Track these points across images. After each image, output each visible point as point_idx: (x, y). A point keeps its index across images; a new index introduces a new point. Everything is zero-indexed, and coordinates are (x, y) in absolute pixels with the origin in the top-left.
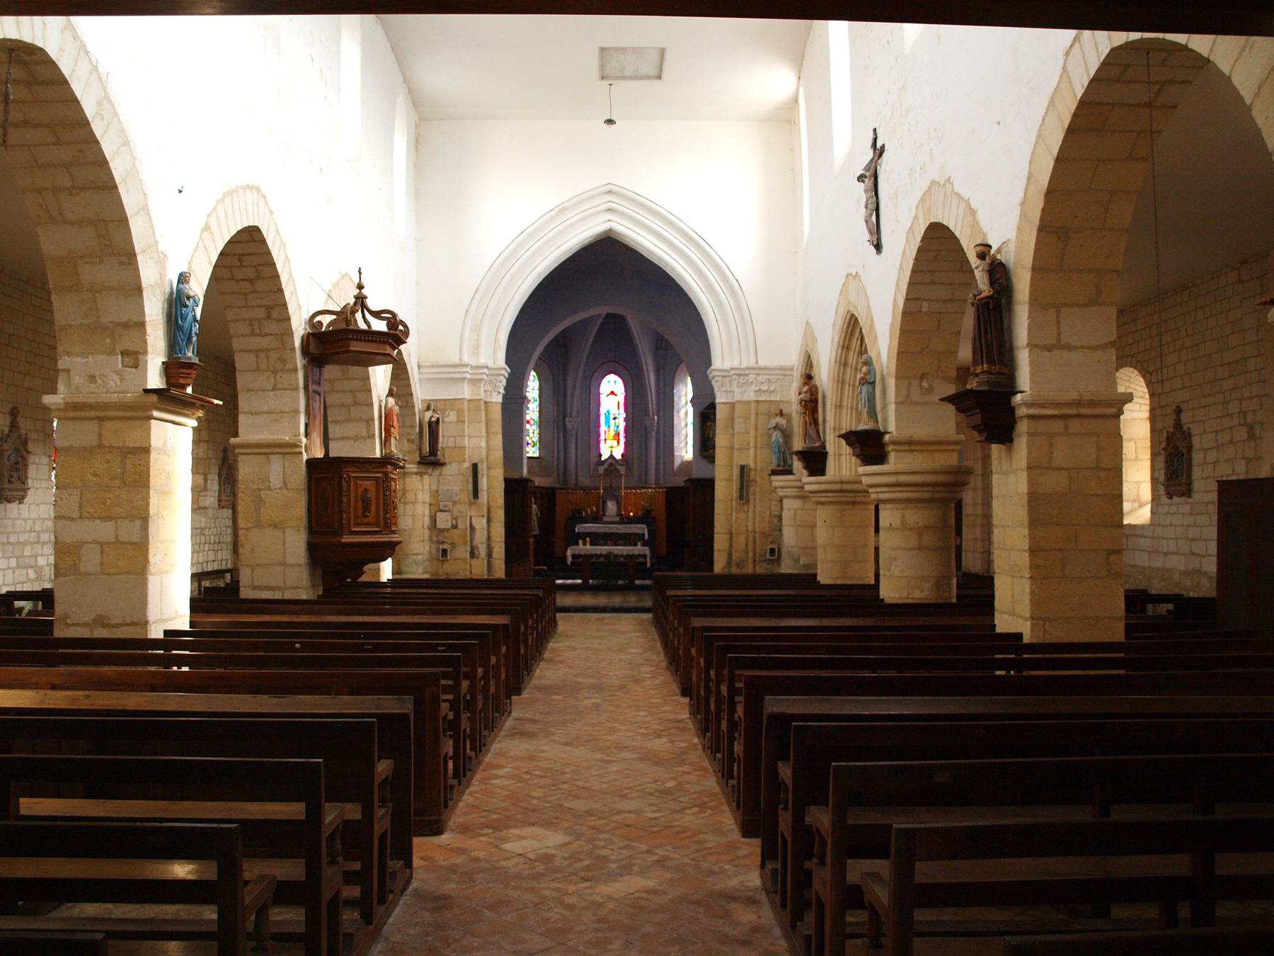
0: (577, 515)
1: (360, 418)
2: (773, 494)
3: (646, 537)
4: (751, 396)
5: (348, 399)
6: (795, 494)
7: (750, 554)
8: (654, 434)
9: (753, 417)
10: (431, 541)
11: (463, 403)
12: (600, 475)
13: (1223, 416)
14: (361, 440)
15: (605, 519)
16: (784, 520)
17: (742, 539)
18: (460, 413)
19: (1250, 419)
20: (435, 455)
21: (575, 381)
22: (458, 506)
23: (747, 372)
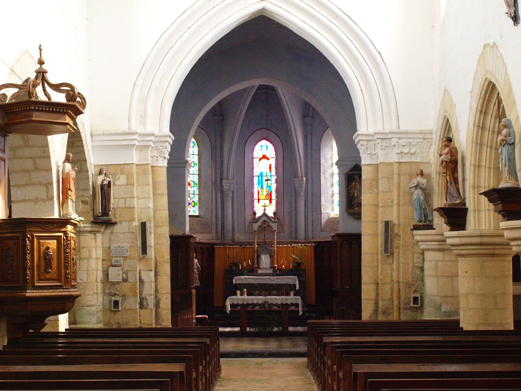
0: (234, 268)
1: (40, 182)
2: (415, 247)
3: (297, 287)
5: (29, 164)
6: (436, 247)
7: (396, 303)
8: (303, 194)
9: (396, 177)
10: (104, 293)
11: (132, 168)
12: (255, 231)
14: (41, 203)
15: (260, 271)
16: (425, 271)
17: (387, 288)
18: (129, 176)
20: (107, 215)
21: (231, 148)
22: (128, 261)
23: (390, 136)
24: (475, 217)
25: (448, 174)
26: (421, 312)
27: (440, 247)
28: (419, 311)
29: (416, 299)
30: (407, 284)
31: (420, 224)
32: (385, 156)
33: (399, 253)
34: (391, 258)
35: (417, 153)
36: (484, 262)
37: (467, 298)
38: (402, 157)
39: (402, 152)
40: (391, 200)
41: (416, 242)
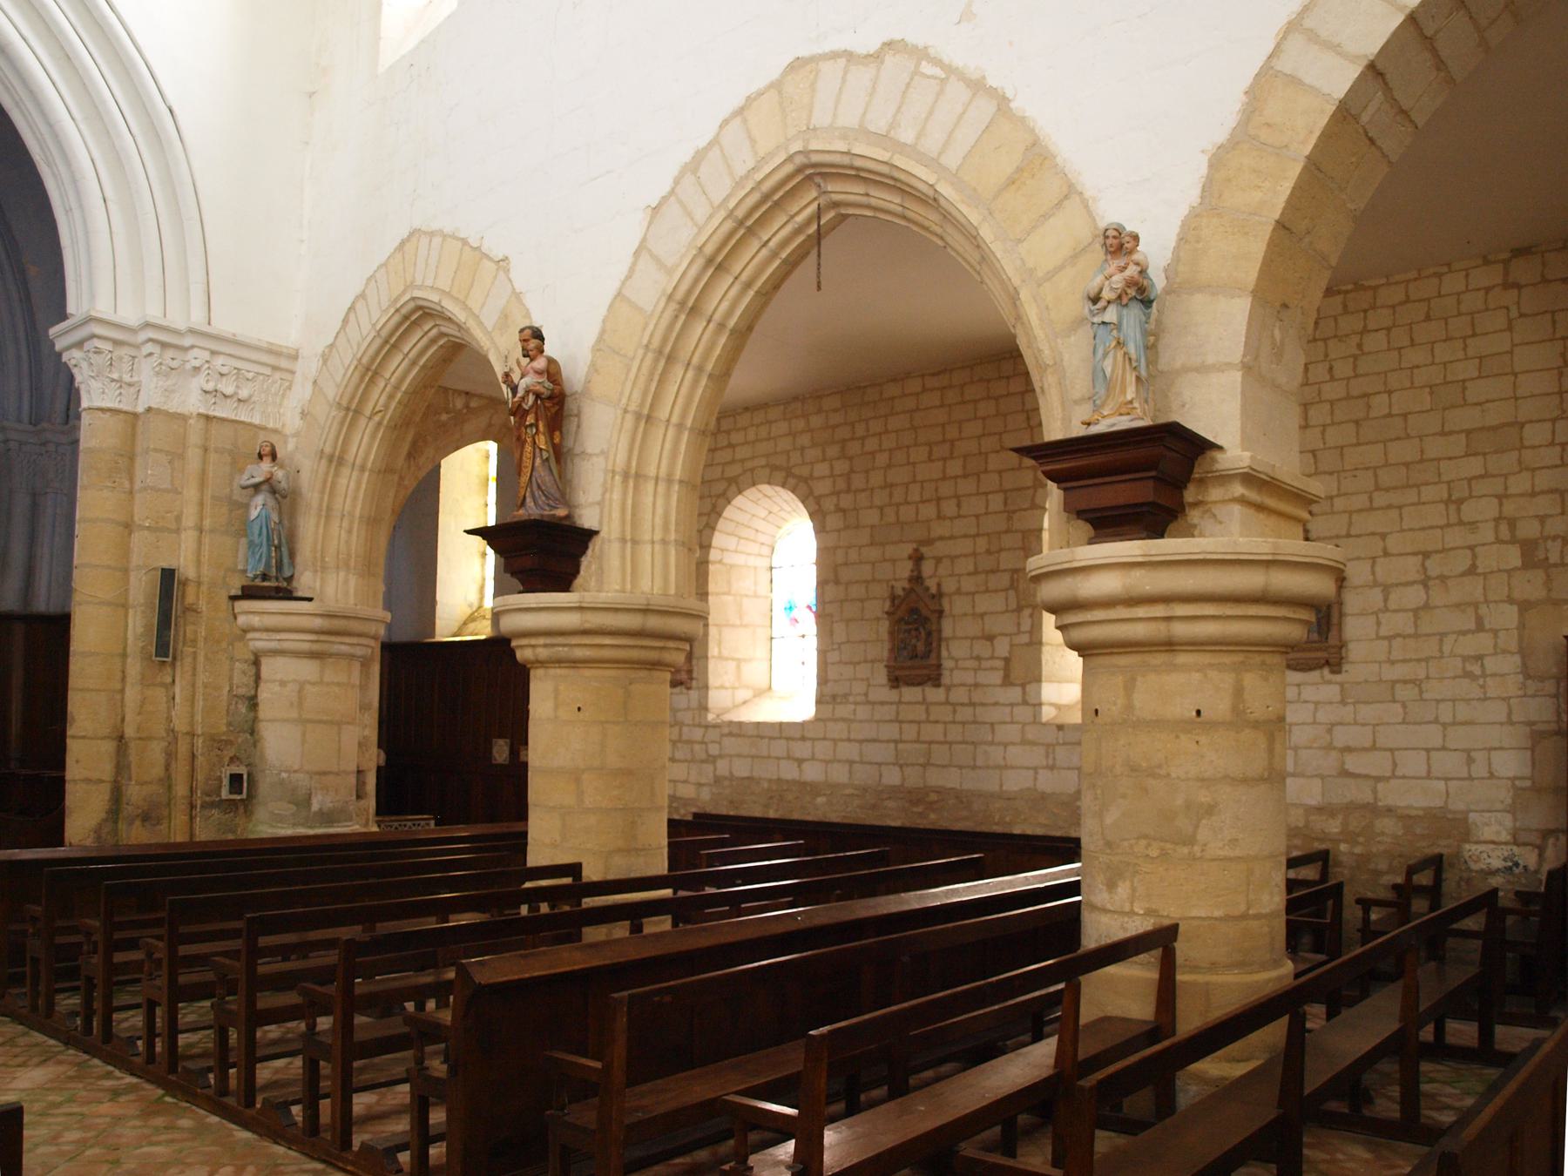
2: (238, 645)
4: (190, 400)
6: (306, 646)
7: (181, 790)
9: (193, 454)
13: (1448, 525)
16: (261, 707)
17: (156, 751)
19: (1529, 530)
23: (187, 342)
24: (623, 558)
25: (541, 428)
26: (245, 812)
27: (315, 647)
28: (241, 810)
29: (236, 780)
30: (214, 740)
31: (266, 584)
32: (167, 394)
33: (195, 658)
34: (169, 670)
35: (254, 402)
36: (630, 684)
37: (578, 780)
38: (215, 403)
39: (216, 391)
40: (175, 513)
41: (239, 632)
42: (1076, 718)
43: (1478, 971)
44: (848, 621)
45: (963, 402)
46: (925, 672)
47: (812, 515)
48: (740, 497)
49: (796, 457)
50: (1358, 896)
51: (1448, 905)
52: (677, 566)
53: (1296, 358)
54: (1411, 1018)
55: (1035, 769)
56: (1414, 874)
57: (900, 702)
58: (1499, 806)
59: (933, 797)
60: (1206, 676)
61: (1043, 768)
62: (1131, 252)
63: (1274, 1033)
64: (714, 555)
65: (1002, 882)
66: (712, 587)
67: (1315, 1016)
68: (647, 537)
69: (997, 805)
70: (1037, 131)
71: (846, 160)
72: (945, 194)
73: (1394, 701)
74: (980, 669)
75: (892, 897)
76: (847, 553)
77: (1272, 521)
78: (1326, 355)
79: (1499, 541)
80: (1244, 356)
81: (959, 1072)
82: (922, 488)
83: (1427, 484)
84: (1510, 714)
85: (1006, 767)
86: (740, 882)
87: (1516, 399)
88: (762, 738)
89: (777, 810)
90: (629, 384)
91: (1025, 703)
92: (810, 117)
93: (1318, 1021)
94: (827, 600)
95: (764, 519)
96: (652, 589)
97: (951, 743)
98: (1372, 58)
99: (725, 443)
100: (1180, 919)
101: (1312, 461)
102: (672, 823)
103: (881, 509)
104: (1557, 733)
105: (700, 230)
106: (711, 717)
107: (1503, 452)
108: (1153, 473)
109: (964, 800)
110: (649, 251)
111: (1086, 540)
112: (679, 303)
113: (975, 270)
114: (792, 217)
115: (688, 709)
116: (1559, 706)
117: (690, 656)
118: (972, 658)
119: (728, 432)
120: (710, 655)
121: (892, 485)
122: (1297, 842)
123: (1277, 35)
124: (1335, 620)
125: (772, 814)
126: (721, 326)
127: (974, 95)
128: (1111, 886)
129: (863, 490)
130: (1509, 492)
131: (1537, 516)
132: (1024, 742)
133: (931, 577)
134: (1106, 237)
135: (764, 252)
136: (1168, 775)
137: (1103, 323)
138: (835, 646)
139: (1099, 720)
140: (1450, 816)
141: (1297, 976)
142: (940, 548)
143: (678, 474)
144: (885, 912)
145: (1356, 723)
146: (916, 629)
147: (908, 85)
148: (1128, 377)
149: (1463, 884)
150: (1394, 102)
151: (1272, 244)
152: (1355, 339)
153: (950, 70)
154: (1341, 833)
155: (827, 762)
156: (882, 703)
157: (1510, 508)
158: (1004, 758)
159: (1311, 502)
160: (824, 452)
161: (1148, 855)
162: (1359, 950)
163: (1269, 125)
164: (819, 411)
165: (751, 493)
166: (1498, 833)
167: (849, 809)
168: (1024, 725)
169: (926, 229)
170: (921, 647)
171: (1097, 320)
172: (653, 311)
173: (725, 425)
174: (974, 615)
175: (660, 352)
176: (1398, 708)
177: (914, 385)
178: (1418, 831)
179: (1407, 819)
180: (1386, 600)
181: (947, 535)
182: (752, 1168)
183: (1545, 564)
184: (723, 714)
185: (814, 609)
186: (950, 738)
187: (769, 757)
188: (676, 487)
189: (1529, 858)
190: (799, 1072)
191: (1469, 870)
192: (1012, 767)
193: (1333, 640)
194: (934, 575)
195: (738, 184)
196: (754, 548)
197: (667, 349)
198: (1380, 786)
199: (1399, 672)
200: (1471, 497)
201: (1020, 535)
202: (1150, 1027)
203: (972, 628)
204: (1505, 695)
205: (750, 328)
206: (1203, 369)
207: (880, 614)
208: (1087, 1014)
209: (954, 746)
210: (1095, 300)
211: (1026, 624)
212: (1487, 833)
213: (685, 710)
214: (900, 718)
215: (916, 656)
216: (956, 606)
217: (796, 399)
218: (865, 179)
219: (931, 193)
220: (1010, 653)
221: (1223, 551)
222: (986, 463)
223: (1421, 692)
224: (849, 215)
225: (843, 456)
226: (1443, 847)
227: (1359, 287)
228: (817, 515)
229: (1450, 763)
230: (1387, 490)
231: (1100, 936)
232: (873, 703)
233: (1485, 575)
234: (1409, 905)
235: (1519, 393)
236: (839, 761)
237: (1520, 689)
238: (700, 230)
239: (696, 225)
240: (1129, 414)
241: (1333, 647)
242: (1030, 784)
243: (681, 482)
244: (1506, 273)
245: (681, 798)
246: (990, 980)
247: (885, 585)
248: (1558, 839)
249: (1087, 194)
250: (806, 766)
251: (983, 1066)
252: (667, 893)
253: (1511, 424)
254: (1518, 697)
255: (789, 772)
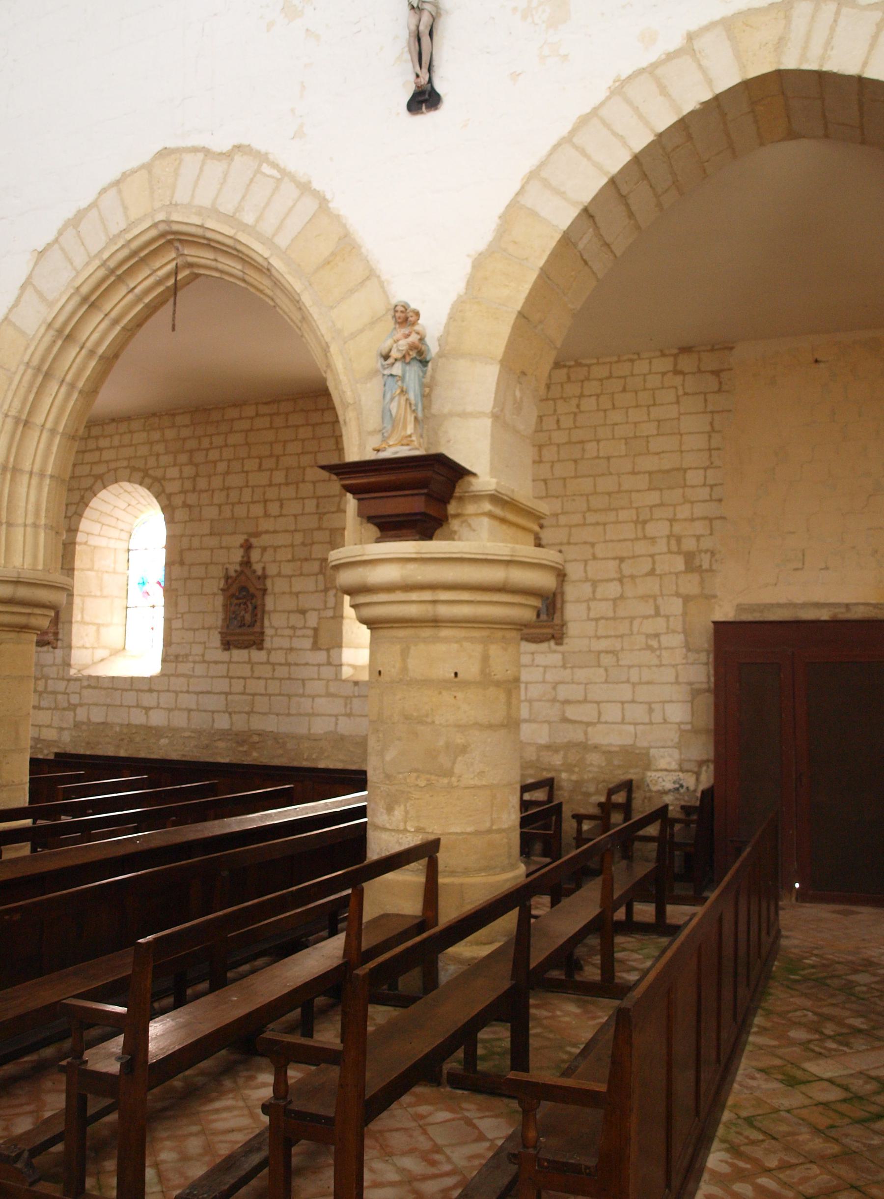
13: (637, 539)
19: (689, 545)
42: (365, 676)
43: (655, 866)
44: (190, 595)
45: (287, 427)
46: (252, 638)
47: (163, 509)
48: (104, 491)
49: (152, 462)
50: (574, 813)
51: (636, 817)
52: (45, 546)
53: (531, 413)
54: (608, 905)
55: (336, 716)
56: (613, 794)
57: (230, 662)
58: (670, 744)
59: (256, 738)
60: (461, 646)
61: (342, 715)
62: (414, 324)
63: (509, 921)
64: (80, 538)
65: (306, 807)
66: (78, 564)
67: (541, 905)
68: (20, 521)
69: (306, 745)
70: (348, 226)
71: (200, 232)
72: (275, 265)
73: (599, 666)
74: (294, 636)
75: (216, 822)
76: (191, 540)
77: (510, 531)
78: (555, 410)
79: (670, 552)
80: (494, 407)
81: (269, 965)
82: (253, 492)
83: (622, 508)
84: (677, 677)
85: (314, 715)
86: (91, 811)
87: (682, 452)
88: (116, 689)
89: (126, 750)
90: (10, 395)
91: (329, 664)
92: (172, 197)
93: (545, 908)
94: (174, 577)
95: (124, 510)
96: (23, 565)
97: (270, 695)
98: (586, 204)
99: (94, 446)
100: (441, 834)
101: (544, 487)
102: (34, 762)
103: (220, 506)
104: (708, 691)
105: (78, 273)
106: (73, 672)
107: (673, 488)
108: (425, 491)
109: (280, 741)
110: (34, 286)
111: (375, 538)
112: (57, 331)
113: (297, 326)
114: (155, 271)
115: (54, 665)
116: (709, 671)
117: (56, 621)
118: (288, 627)
119: (97, 438)
120: (74, 620)
121: (228, 488)
122: (531, 772)
123: (522, 179)
124: (559, 605)
125: (122, 753)
126: (92, 352)
127: (302, 193)
128: (390, 809)
129: (206, 491)
130: (677, 517)
131: (695, 535)
132: (329, 695)
133: (257, 562)
134: (396, 311)
135: (131, 297)
136: (433, 722)
137: (391, 375)
138: (179, 616)
139: (382, 679)
140: (637, 751)
141: (528, 876)
142: (265, 540)
143: (49, 471)
144: (211, 835)
145: (573, 683)
146: (245, 604)
147: (252, 180)
148: (409, 419)
149: (646, 801)
150: (599, 235)
151: (515, 328)
152: (574, 402)
153: (284, 172)
154: (563, 765)
155: (170, 710)
156: (216, 662)
157: (677, 529)
158: (312, 708)
159: (540, 518)
160: (175, 459)
161: (417, 785)
162: (574, 853)
163: (515, 243)
164: (173, 426)
165: (114, 488)
166: (669, 763)
167: (187, 749)
168: (328, 681)
169: (261, 291)
170: (248, 617)
171: (387, 372)
172: (34, 335)
173: (95, 431)
174: (291, 593)
175: (38, 369)
176: (601, 671)
177: (250, 411)
178: (616, 762)
179: (608, 753)
180: (594, 592)
181: (272, 529)
182: (87, 1061)
183: (699, 570)
184: (83, 670)
185: (163, 584)
186: (270, 691)
187: (121, 706)
188: (47, 481)
189: (689, 781)
190: (128, 976)
191: (650, 791)
192: (318, 715)
193: (557, 621)
194: (260, 561)
195: (112, 240)
196: (114, 533)
197: (45, 368)
198: (590, 729)
199: (603, 644)
200: (652, 519)
201: (328, 532)
202: (416, 921)
203: (289, 603)
204: (673, 663)
205: (116, 356)
206: (464, 415)
207: (216, 590)
208: (369, 913)
209: (272, 698)
210: (386, 357)
211: (331, 602)
212: (663, 764)
213: (51, 666)
214: (230, 674)
215: (244, 625)
216: (276, 586)
217: (154, 415)
218: (214, 248)
219: (265, 264)
220: (318, 624)
221: (475, 552)
222: (304, 474)
223: (618, 660)
224: (201, 275)
225: (191, 462)
226: (633, 774)
227: (578, 364)
228: (168, 509)
229: (638, 712)
230: (595, 511)
231: (381, 849)
232: (209, 662)
233: (660, 576)
234: (609, 818)
235: (684, 448)
236: (180, 709)
237: (684, 658)
238: (78, 273)
239: (75, 269)
240: (408, 445)
241: (557, 625)
242: (331, 728)
243: (52, 477)
244: (675, 364)
245: (44, 740)
246: (290, 889)
247: (220, 567)
248: (708, 767)
249: (383, 278)
250: (151, 713)
251: (286, 960)
252: (28, 822)
253: (677, 469)
254: (683, 664)
255: (138, 718)
